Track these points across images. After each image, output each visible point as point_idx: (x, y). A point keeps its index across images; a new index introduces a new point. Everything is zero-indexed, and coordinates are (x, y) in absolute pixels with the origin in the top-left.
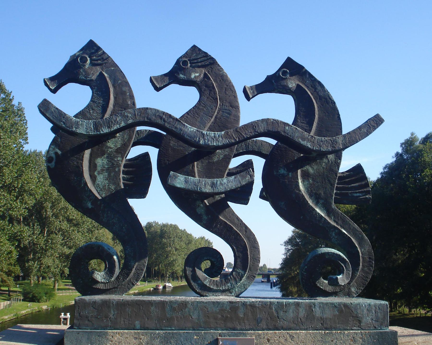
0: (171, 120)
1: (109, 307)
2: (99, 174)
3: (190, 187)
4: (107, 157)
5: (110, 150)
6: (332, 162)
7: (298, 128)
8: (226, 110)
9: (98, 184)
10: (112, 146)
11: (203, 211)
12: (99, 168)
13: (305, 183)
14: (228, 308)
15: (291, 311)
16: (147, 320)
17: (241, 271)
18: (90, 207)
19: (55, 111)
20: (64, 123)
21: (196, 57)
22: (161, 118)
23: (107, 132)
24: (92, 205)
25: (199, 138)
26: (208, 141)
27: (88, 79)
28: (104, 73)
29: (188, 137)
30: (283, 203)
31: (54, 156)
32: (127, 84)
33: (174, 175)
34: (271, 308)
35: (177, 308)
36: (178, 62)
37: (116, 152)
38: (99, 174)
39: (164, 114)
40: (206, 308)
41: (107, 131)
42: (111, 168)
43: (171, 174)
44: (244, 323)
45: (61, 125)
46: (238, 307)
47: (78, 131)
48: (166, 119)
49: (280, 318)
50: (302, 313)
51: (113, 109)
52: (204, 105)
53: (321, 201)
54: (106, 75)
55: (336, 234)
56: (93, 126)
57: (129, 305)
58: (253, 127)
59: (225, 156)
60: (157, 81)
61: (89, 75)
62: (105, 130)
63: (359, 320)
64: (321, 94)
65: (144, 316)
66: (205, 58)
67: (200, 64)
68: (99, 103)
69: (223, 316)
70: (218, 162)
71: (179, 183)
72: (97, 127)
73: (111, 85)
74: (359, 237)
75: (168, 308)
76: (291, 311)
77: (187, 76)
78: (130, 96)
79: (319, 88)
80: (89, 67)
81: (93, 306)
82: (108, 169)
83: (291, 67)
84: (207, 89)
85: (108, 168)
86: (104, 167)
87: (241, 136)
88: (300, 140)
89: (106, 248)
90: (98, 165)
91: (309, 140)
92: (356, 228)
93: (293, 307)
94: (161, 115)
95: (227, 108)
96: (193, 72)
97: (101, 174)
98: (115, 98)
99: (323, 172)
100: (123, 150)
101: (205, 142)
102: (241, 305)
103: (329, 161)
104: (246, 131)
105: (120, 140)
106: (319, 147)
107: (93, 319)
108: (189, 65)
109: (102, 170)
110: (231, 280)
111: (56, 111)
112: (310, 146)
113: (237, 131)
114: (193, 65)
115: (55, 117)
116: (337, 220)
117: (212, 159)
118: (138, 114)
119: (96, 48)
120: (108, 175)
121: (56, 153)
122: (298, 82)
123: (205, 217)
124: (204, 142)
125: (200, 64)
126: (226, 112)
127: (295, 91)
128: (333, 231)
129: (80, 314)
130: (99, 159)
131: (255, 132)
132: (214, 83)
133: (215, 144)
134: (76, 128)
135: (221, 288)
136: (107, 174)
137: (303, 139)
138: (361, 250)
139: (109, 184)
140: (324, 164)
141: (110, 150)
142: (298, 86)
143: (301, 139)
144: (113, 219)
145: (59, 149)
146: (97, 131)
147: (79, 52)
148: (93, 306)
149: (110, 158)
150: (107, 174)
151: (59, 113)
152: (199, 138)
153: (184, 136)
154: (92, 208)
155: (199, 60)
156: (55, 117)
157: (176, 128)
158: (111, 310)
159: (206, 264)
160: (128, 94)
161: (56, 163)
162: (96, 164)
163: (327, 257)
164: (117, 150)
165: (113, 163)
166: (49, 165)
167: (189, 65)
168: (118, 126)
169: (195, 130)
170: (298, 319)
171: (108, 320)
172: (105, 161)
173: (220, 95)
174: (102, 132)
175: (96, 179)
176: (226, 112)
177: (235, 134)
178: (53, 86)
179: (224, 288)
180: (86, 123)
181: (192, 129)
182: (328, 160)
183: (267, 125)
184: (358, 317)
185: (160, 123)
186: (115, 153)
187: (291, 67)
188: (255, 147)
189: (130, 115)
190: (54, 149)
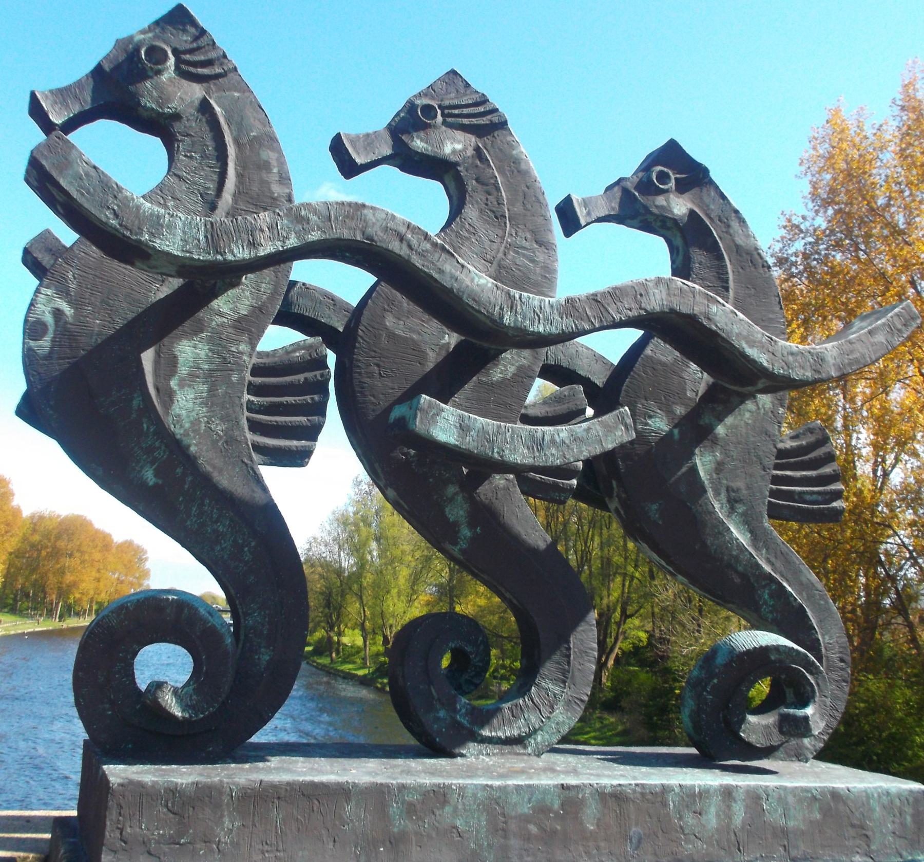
0: (428, 246)
1: (217, 806)
2: (181, 385)
3: (470, 443)
4: (210, 341)
5: (220, 320)
6: (766, 413)
7: (738, 313)
8: (524, 248)
9: (179, 416)
10: (225, 309)
11: (461, 513)
12: (183, 370)
13: (704, 459)
14: (556, 805)
15: (713, 810)
16: (331, 844)
17: (551, 686)
18: (151, 483)
19: (87, 174)
20: (116, 215)
21: (456, 102)
22: (402, 238)
23: (244, 259)
24: (156, 475)
25: (501, 309)
26: (524, 318)
27: (166, 110)
28: (212, 102)
29: (471, 303)
30: (654, 507)
31: (49, 319)
32: (271, 140)
33: (430, 405)
34: (665, 804)
35: (418, 806)
36: (410, 107)
37: (235, 327)
38: (181, 385)
39: (408, 227)
40: (498, 804)
41: (247, 256)
42: (219, 373)
43: (422, 401)
44: (598, 848)
45: (104, 219)
46: (583, 801)
47: (158, 244)
48: (414, 242)
49: (686, 832)
50: (739, 814)
51: (232, 207)
52: (472, 230)
53: (741, 508)
54: (218, 109)
55: (771, 596)
56: (206, 237)
57: (279, 798)
58: (635, 297)
59: (520, 368)
60: (354, 148)
61: (169, 100)
62: (241, 253)
63: (867, 836)
64: (740, 241)
65: (324, 832)
66: (481, 109)
67: (466, 121)
68: (195, 183)
69: (542, 829)
70: (504, 382)
71: (444, 430)
72: (214, 238)
73: (231, 140)
74: (819, 605)
75: (394, 808)
76: (713, 810)
77: (432, 146)
78: (281, 177)
79: (735, 225)
80: (170, 79)
81: (167, 806)
82: (209, 374)
83: (675, 165)
84: (479, 187)
85: (210, 370)
86: (199, 368)
87: (605, 314)
88: (745, 345)
89: (202, 611)
90: (181, 360)
91: (762, 347)
92: (814, 582)
93: (716, 800)
94: (403, 230)
95: (527, 245)
96: (449, 139)
97: (190, 386)
98: (239, 176)
99: (747, 433)
100: (250, 326)
101: (516, 320)
102: (591, 794)
103: (759, 408)
104: (619, 304)
105: (247, 293)
106: (786, 368)
107: (166, 848)
108: (439, 118)
109: (192, 376)
110: (525, 710)
111: (93, 172)
112: (765, 364)
113: (597, 301)
114: (450, 120)
115: (88, 192)
116: (773, 560)
117: (488, 375)
118: (336, 219)
119: (192, 30)
120: (209, 391)
121: (58, 313)
122: (690, 206)
123: (466, 532)
124: (513, 319)
125: (466, 121)
126: (524, 256)
127: (684, 225)
128: (764, 587)
129: (121, 830)
130: (185, 342)
131: (641, 308)
132: (497, 174)
133: (541, 329)
134: (152, 234)
135: (500, 734)
136: (205, 388)
137: (752, 344)
138: (824, 639)
139: (209, 418)
140: (747, 415)
141: (220, 320)
142: (692, 213)
143: (747, 342)
144: (216, 522)
145: (69, 303)
146: (217, 252)
147: (143, 32)
148: (167, 806)
149: (218, 342)
150: (205, 388)
151: (101, 181)
152: (501, 309)
153: (461, 299)
154: (156, 485)
155: (466, 111)
156: (88, 192)
157: (441, 271)
158: (222, 816)
159: (496, 674)
160: (275, 170)
161: (53, 341)
162: (175, 357)
163: (773, 658)
164: (238, 321)
165: (225, 358)
166: (32, 343)
167: (439, 118)
168: (279, 244)
169: (490, 285)
170: (728, 833)
171: (212, 850)
172: (203, 351)
173: (510, 207)
174: (230, 257)
175: (172, 401)
176: (524, 256)
177: (591, 308)
178: (59, 114)
179: (508, 734)
180: (184, 224)
181: (482, 281)
182: (757, 405)
183: (669, 294)
184: (862, 827)
185: (397, 251)
186: (230, 330)
187: (675, 165)
188: (563, 358)
189: (315, 218)
190: (50, 299)
